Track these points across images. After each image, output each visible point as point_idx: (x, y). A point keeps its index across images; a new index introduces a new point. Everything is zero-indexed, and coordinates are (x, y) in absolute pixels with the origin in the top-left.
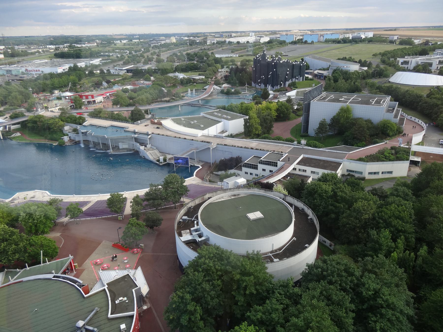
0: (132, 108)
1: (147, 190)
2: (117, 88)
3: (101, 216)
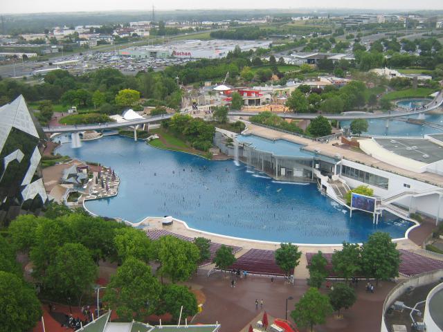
0: (314, 117)
1: (339, 247)
2: (292, 86)
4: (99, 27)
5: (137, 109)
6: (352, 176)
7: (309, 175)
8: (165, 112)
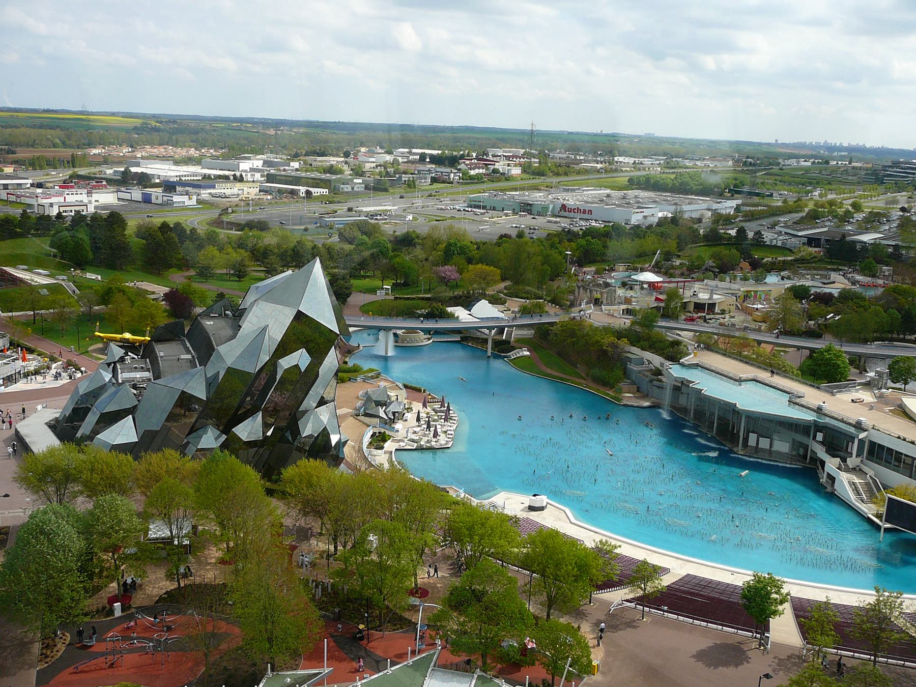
3: (693, 619)
4: (435, 152)
5: (494, 301)
6: (887, 464)
7: (801, 451)
8: (540, 310)
